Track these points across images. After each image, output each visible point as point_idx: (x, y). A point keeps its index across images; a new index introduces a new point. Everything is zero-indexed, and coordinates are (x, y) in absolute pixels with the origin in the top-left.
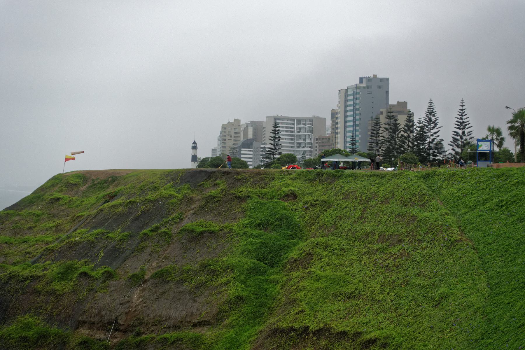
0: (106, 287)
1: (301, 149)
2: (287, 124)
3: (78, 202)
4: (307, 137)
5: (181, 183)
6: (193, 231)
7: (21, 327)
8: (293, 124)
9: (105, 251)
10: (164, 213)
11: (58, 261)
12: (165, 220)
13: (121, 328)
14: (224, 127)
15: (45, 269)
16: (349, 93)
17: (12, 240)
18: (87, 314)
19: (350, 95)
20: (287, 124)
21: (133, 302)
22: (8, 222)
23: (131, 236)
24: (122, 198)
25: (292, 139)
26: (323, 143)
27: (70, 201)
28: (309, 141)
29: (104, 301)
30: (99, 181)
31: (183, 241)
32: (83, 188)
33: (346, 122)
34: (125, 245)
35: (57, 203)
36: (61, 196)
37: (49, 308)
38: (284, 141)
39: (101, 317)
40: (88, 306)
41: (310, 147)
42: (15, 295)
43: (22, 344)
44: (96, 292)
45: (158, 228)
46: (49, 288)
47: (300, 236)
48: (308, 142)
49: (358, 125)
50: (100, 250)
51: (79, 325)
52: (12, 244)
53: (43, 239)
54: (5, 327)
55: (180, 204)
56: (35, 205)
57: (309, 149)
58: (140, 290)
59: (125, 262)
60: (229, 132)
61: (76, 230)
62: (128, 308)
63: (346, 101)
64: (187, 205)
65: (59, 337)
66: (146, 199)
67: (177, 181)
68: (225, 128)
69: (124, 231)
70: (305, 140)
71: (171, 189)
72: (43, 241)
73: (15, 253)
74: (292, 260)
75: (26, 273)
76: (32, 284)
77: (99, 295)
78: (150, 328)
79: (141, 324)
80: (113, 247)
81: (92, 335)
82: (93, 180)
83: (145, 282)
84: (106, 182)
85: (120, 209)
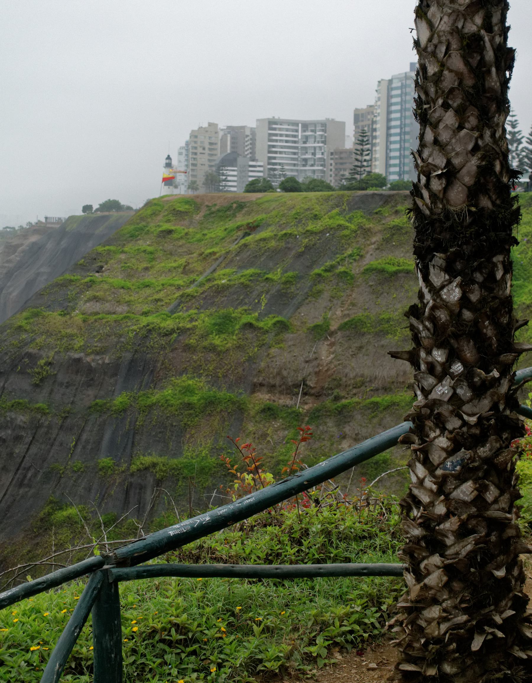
0: (282, 341)
1: (307, 168)
2: (287, 130)
3: (198, 236)
4: (317, 151)
5: (350, 210)
6: (382, 271)
7: (180, 391)
8: (297, 131)
9: (268, 296)
10: (336, 249)
11: (206, 309)
12: (339, 257)
13: (313, 391)
14: (194, 135)
15: (192, 320)
16: (394, 85)
17: (129, 284)
18: (263, 375)
19: (396, 88)
20: (287, 130)
21: (322, 360)
22: (112, 261)
23: (299, 278)
24: (270, 229)
25: (295, 154)
26: (341, 158)
27: (187, 234)
28: (320, 156)
29: (282, 358)
30: (217, 207)
31: (371, 283)
32: (198, 217)
33: (389, 128)
34: (293, 289)
35: (170, 236)
36: (173, 228)
37: (211, 368)
38: (284, 156)
39: (283, 378)
40: (263, 364)
41: (322, 165)
42: (162, 353)
43: (186, 412)
44: (270, 347)
45: (333, 267)
46: (206, 343)
47: (525, 277)
48: (320, 158)
49: (408, 133)
50: (259, 295)
51: (255, 387)
52: (129, 288)
53: (171, 282)
54: (157, 393)
55: (355, 237)
56: (140, 239)
57: (321, 168)
58: (327, 345)
59: (299, 310)
60: (202, 142)
61: (215, 270)
62: (318, 367)
63: (389, 97)
64: (365, 238)
65: (233, 403)
66: (307, 231)
67: (344, 207)
68: (196, 137)
69: (286, 272)
70: (314, 154)
71: (337, 217)
72: (171, 285)
73: (140, 300)
74: (524, 306)
75: (169, 324)
76: (181, 338)
77: (273, 351)
78: (350, 390)
79: (339, 386)
80: (279, 291)
81: (274, 401)
82: (207, 206)
83: (332, 334)
84: (229, 208)
85: (273, 244)
